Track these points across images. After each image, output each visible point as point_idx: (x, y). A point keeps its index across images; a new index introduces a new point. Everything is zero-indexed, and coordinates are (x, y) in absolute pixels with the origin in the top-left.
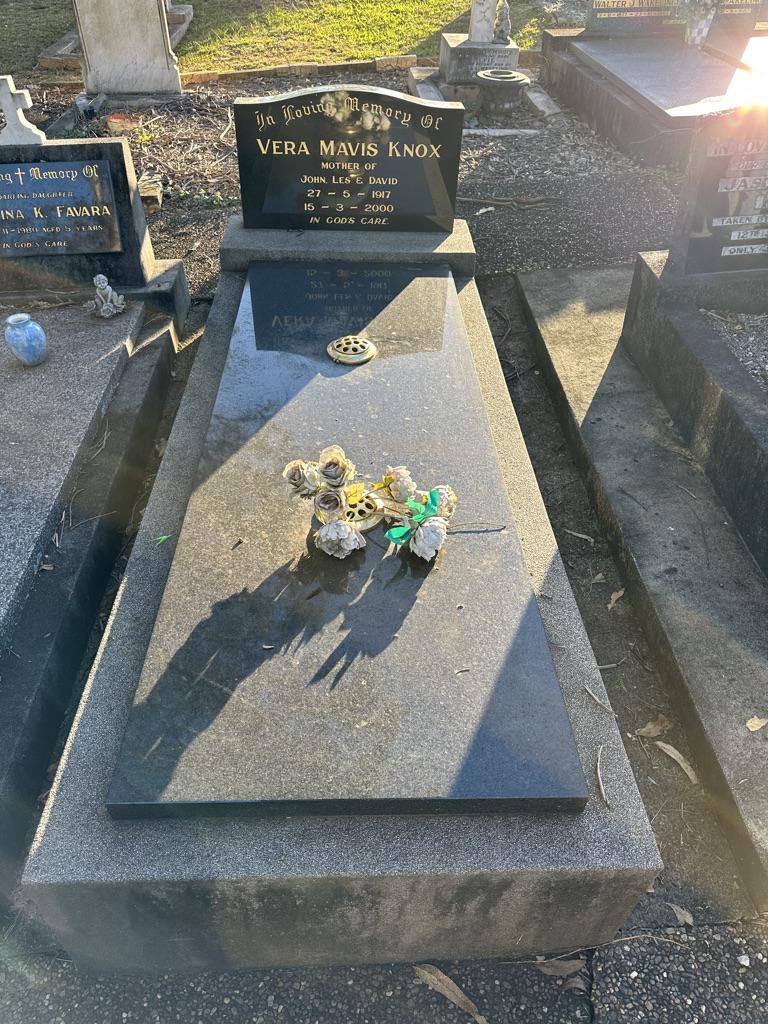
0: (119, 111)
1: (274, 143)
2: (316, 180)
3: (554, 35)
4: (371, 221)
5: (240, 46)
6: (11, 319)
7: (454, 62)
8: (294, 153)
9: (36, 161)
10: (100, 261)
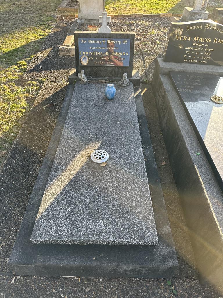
0: (90, 25)
1: (181, 37)
2: (190, 48)
3: (219, 9)
4: (202, 62)
5: (116, 7)
6: (109, 85)
7: (189, 16)
8: (186, 40)
9: (109, 38)
10: (121, 69)
